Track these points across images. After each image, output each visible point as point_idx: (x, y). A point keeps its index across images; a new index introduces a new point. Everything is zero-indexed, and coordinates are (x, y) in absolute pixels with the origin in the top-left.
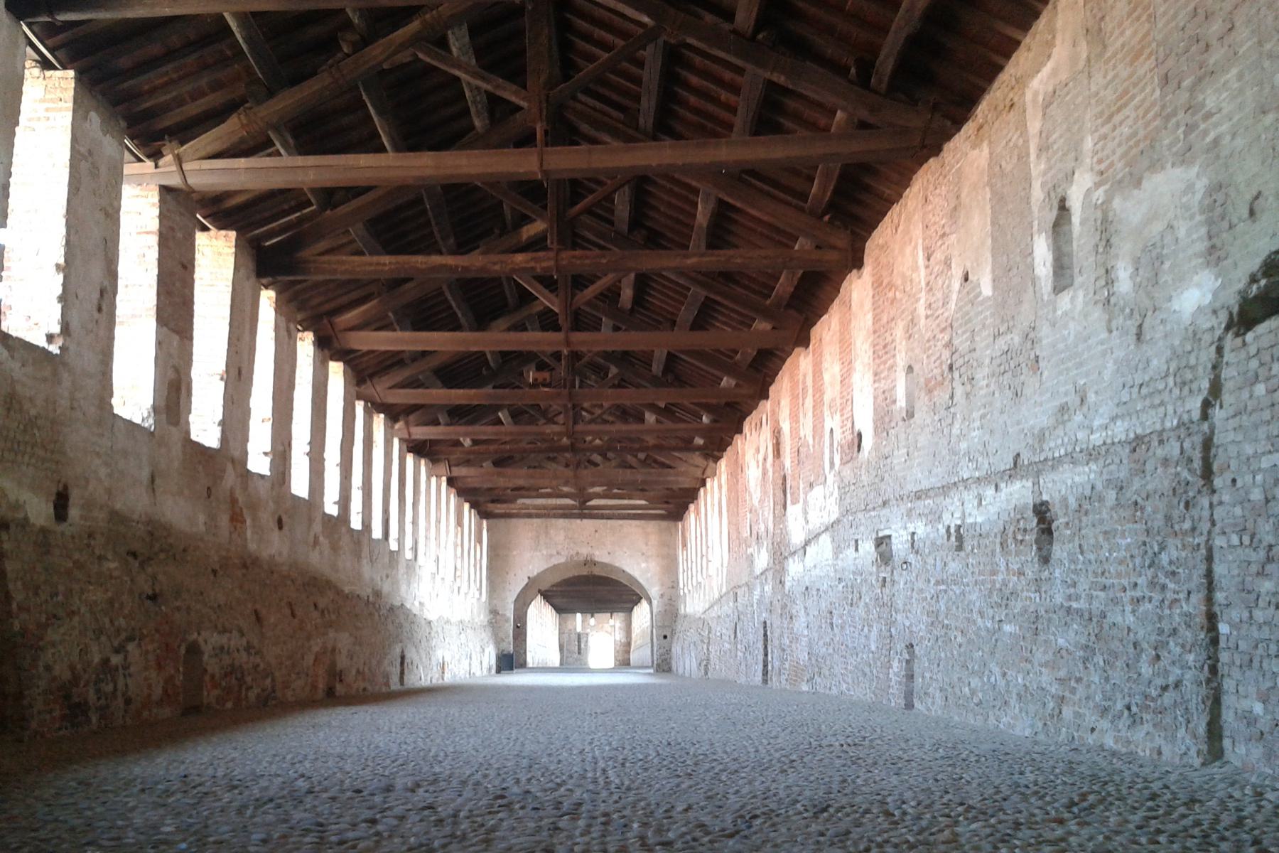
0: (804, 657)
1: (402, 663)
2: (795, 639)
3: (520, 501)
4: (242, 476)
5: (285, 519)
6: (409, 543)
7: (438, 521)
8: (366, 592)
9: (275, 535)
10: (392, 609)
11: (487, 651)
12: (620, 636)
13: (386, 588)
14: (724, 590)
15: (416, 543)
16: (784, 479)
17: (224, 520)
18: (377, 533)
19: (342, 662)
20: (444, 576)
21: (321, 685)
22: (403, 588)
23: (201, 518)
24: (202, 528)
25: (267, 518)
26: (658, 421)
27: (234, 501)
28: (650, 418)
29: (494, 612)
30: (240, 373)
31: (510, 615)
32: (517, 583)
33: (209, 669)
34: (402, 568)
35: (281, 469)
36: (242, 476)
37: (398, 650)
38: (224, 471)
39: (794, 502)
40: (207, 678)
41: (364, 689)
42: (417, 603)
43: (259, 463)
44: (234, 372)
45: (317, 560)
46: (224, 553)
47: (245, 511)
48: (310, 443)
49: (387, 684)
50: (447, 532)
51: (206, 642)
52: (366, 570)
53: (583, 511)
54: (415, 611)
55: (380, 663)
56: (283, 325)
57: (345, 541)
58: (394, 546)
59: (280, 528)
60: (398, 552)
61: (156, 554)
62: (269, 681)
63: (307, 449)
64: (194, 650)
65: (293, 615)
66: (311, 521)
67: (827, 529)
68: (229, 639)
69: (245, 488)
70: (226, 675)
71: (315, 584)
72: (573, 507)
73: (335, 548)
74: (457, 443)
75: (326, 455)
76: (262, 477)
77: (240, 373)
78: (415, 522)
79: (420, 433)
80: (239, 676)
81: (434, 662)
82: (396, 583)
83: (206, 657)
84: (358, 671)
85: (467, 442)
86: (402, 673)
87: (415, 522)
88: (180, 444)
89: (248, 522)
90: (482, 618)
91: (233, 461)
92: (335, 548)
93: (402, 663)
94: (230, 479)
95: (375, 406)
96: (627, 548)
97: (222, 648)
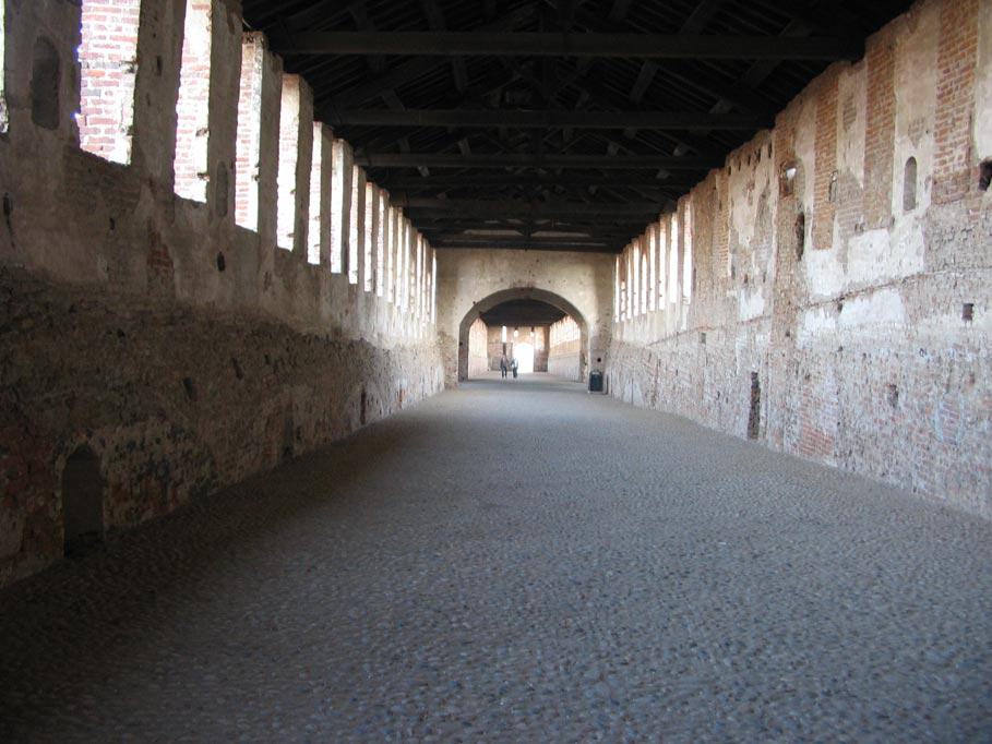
0: (829, 426)
1: (363, 401)
2: (812, 402)
3: (467, 232)
4: (166, 203)
5: (228, 256)
6: (368, 275)
7: (395, 251)
8: (324, 331)
9: (215, 278)
10: (351, 345)
11: (437, 370)
12: (540, 345)
13: (346, 323)
14: (684, 327)
15: (374, 274)
16: (802, 219)
17: (139, 263)
18: (336, 267)
19: (300, 417)
20: (407, 309)
21: (276, 451)
22: (363, 322)
23: (101, 263)
24: (103, 275)
25: (202, 256)
26: (620, 152)
27: (153, 237)
28: (612, 149)
29: (442, 334)
30: (159, 64)
31: (456, 336)
32: (463, 307)
33: (112, 478)
34: (361, 303)
35: (222, 195)
36: (166, 203)
37: (358, 389)
38: (138, 196)
39: (822, 244)
40: (107, 492)
41: (325, 440)
42: (375, 336)
43: (191, 187)
44: (150, 63)
45: (269, 302)
46: (140, 307)
47: (171, 250)
48: (259, 165)
49: (349, 428)
50: (403, 261)
51: (103, 443)
52: (326, 309)
53: (526, 243)
54: (374, 344)
55: (341, 408)
56: (223, 13)
57: (302, 280)
58: (353, 279)
59: (222, 267)
60: (357, 286)
61: (18, 320)
62: (206, 468)
63: (256, 172)
64: (84, 456)
65: (239, 375)
66: (261, 258)
67: (892, 283)
68: (143, 430)
69: (170, 219)
70: (140, 478)
71: (265, 332)
72: (517, 238)
73: (290, 288)
74: (416, 173)
75: (279, 181)
76: (194, 204)
77: (159, 64)
78: (374, 254)
79: (380, 162)
80: (161, 472)
81: (392, 394)
82: (355, 319)
83: (104, 463)
84: (318, 424)
85: (425, 172)
86: (363, 411)
87: (374, 254)
88: (60, 157)
89: (176, 263)
90: (433, 339)
91: (151, 184)
92: (290, 288)
93: (363, 401)
94: (147, 206)
95: (334, 132)
96: (573, 285)
97: (132, 445)
